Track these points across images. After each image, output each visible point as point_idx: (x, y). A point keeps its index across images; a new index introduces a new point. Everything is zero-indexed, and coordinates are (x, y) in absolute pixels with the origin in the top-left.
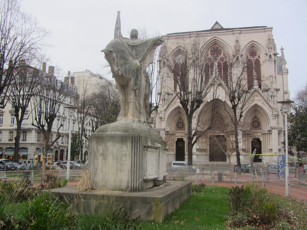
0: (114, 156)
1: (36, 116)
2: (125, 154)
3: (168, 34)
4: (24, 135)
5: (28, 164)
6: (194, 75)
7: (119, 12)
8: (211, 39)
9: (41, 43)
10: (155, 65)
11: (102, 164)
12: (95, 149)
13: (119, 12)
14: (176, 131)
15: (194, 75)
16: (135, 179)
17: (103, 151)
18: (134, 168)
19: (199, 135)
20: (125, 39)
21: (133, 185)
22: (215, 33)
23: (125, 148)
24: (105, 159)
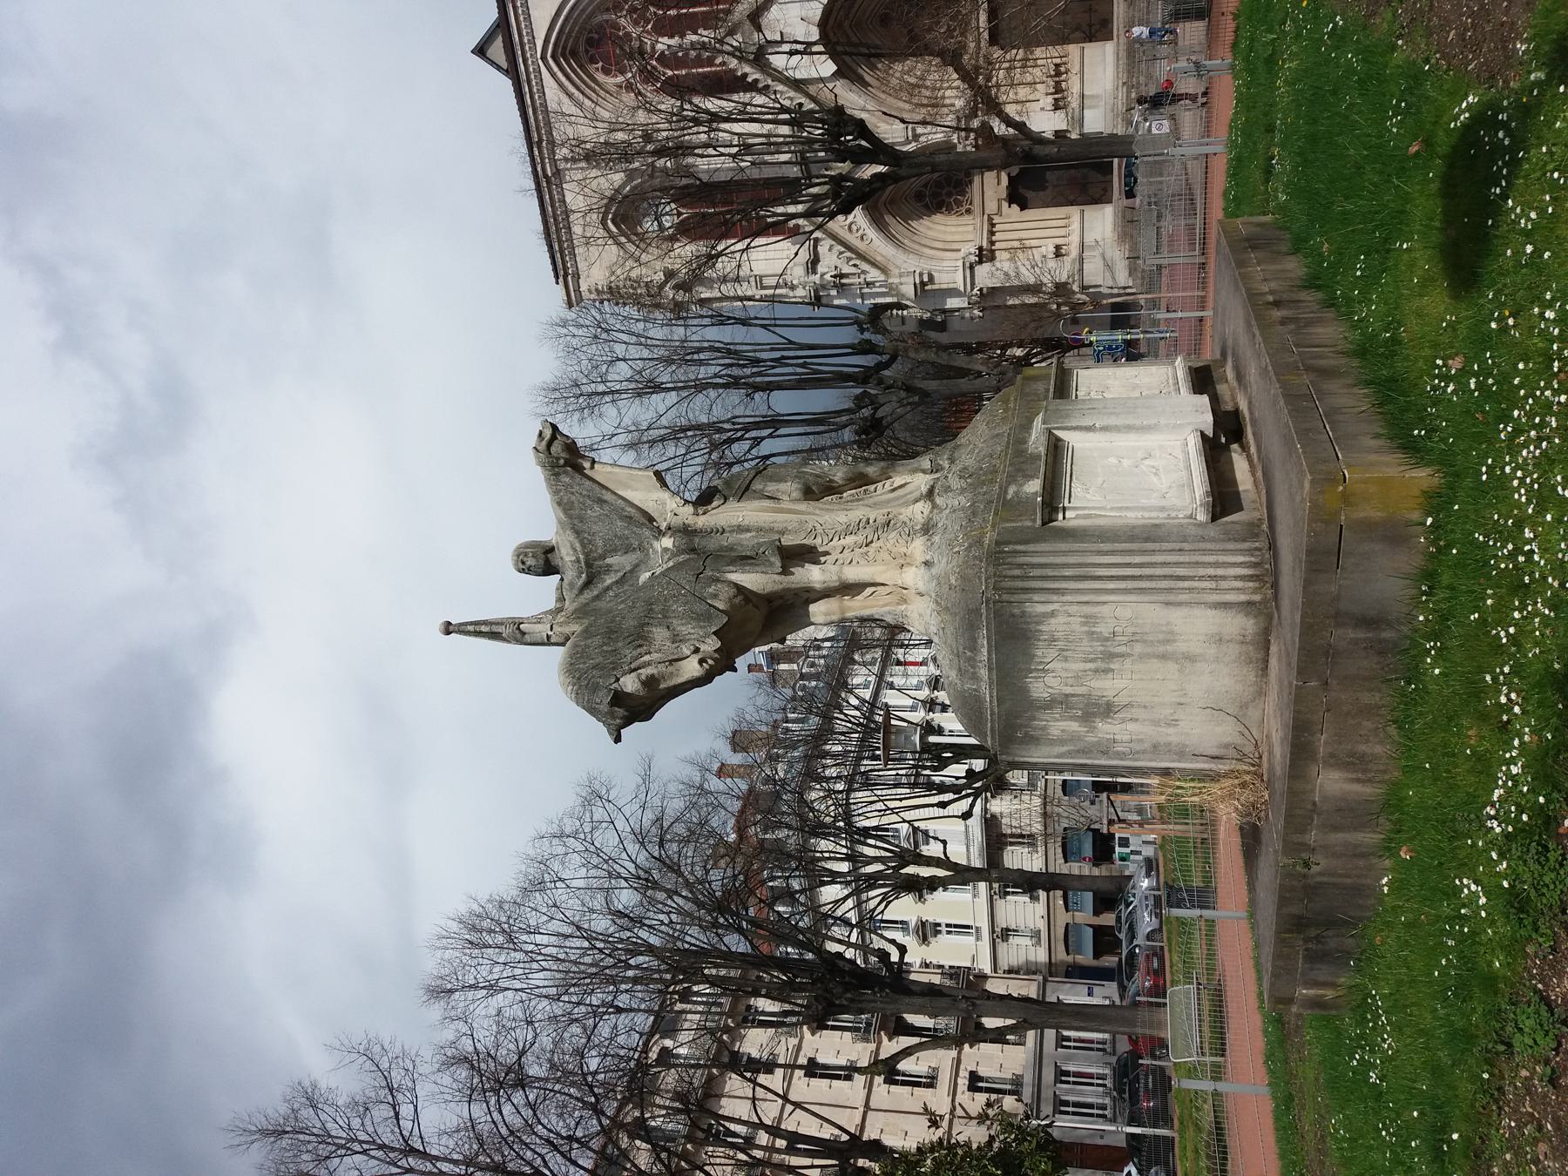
0: (1096, 671)
1: (932, 805)
2: (1084, 624)
3: (557, 277)
4: (1012, 844)
5: (1132, 848)
6: (722, 155)
7: (448, 629)
8: (553, 75)
9: (640, 811)
10: (694, 337)
11: (1137, 720)
12: (1064, 749)
13: (448, 629)
14: (976, 207)
15: (722, 155)
16: (1211, 571)
17: (1073, 718)
18: (1150, 578)
19: (983, 99)
20: (561, 599)
21: (1239, 584)
22: (525, 61)
23: (1053, 621)
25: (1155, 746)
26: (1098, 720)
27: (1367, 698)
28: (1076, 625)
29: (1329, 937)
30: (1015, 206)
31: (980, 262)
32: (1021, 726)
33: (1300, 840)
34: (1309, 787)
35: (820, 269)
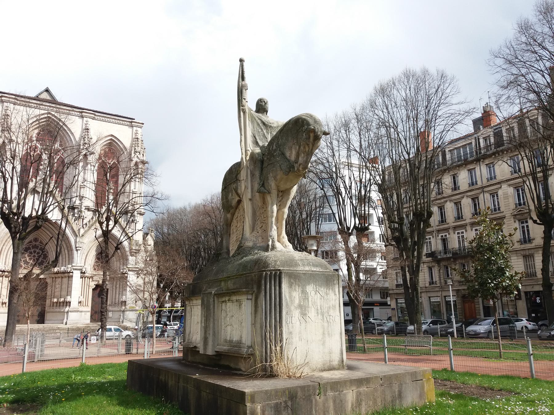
0: (317, 310)
12: (288, 298)
13: (241, 61)
23: (333, 294)
24: (304, 314)
25: (291, 333)
26: (300, 310)
27: (379, 400)
28: (332, 302)
29: (288, 411)
30: (95, 286)
31: (81, 273)
32: (295, 281)
33: (328, 389)
34: (348, 388)
35: (86, 211)
